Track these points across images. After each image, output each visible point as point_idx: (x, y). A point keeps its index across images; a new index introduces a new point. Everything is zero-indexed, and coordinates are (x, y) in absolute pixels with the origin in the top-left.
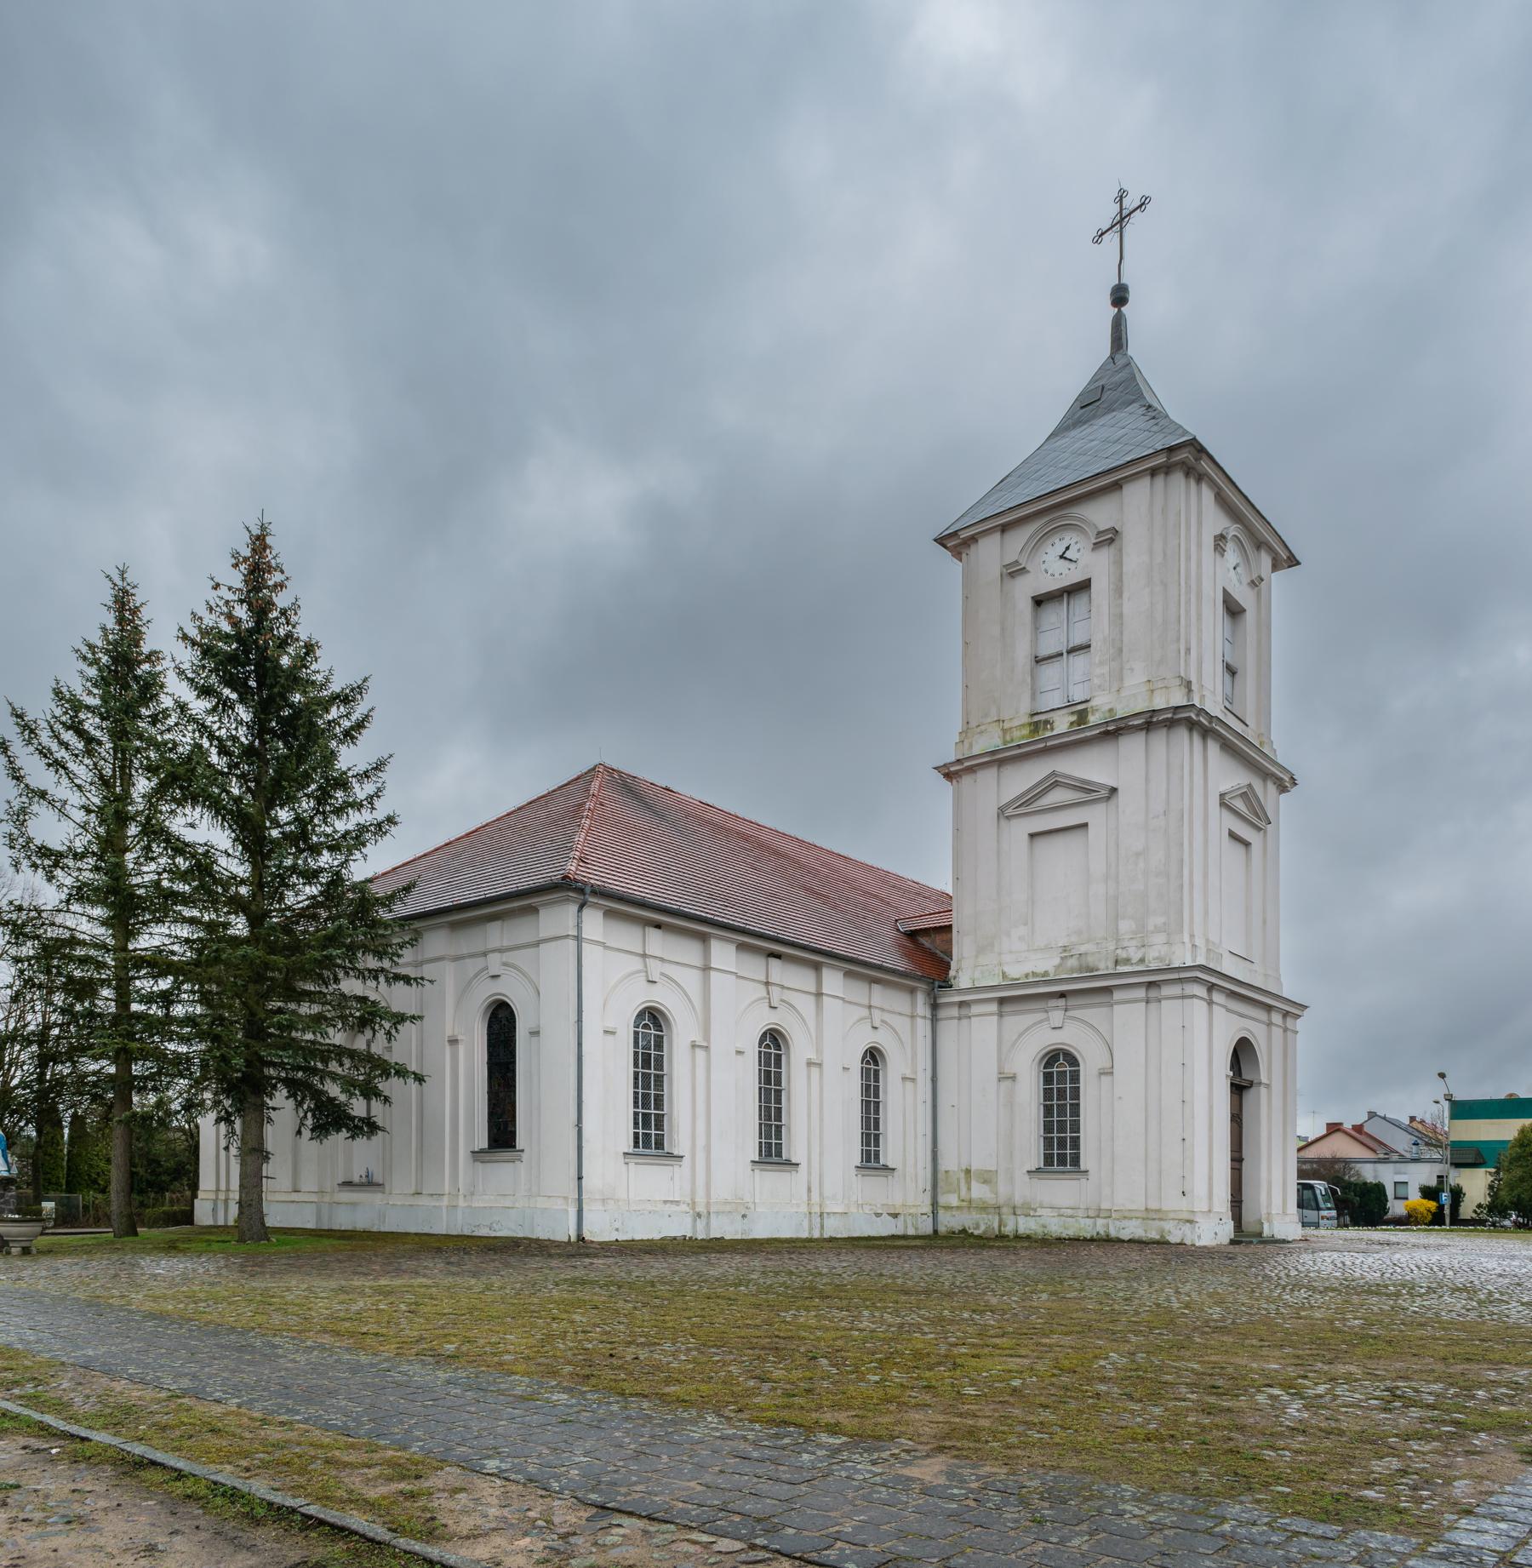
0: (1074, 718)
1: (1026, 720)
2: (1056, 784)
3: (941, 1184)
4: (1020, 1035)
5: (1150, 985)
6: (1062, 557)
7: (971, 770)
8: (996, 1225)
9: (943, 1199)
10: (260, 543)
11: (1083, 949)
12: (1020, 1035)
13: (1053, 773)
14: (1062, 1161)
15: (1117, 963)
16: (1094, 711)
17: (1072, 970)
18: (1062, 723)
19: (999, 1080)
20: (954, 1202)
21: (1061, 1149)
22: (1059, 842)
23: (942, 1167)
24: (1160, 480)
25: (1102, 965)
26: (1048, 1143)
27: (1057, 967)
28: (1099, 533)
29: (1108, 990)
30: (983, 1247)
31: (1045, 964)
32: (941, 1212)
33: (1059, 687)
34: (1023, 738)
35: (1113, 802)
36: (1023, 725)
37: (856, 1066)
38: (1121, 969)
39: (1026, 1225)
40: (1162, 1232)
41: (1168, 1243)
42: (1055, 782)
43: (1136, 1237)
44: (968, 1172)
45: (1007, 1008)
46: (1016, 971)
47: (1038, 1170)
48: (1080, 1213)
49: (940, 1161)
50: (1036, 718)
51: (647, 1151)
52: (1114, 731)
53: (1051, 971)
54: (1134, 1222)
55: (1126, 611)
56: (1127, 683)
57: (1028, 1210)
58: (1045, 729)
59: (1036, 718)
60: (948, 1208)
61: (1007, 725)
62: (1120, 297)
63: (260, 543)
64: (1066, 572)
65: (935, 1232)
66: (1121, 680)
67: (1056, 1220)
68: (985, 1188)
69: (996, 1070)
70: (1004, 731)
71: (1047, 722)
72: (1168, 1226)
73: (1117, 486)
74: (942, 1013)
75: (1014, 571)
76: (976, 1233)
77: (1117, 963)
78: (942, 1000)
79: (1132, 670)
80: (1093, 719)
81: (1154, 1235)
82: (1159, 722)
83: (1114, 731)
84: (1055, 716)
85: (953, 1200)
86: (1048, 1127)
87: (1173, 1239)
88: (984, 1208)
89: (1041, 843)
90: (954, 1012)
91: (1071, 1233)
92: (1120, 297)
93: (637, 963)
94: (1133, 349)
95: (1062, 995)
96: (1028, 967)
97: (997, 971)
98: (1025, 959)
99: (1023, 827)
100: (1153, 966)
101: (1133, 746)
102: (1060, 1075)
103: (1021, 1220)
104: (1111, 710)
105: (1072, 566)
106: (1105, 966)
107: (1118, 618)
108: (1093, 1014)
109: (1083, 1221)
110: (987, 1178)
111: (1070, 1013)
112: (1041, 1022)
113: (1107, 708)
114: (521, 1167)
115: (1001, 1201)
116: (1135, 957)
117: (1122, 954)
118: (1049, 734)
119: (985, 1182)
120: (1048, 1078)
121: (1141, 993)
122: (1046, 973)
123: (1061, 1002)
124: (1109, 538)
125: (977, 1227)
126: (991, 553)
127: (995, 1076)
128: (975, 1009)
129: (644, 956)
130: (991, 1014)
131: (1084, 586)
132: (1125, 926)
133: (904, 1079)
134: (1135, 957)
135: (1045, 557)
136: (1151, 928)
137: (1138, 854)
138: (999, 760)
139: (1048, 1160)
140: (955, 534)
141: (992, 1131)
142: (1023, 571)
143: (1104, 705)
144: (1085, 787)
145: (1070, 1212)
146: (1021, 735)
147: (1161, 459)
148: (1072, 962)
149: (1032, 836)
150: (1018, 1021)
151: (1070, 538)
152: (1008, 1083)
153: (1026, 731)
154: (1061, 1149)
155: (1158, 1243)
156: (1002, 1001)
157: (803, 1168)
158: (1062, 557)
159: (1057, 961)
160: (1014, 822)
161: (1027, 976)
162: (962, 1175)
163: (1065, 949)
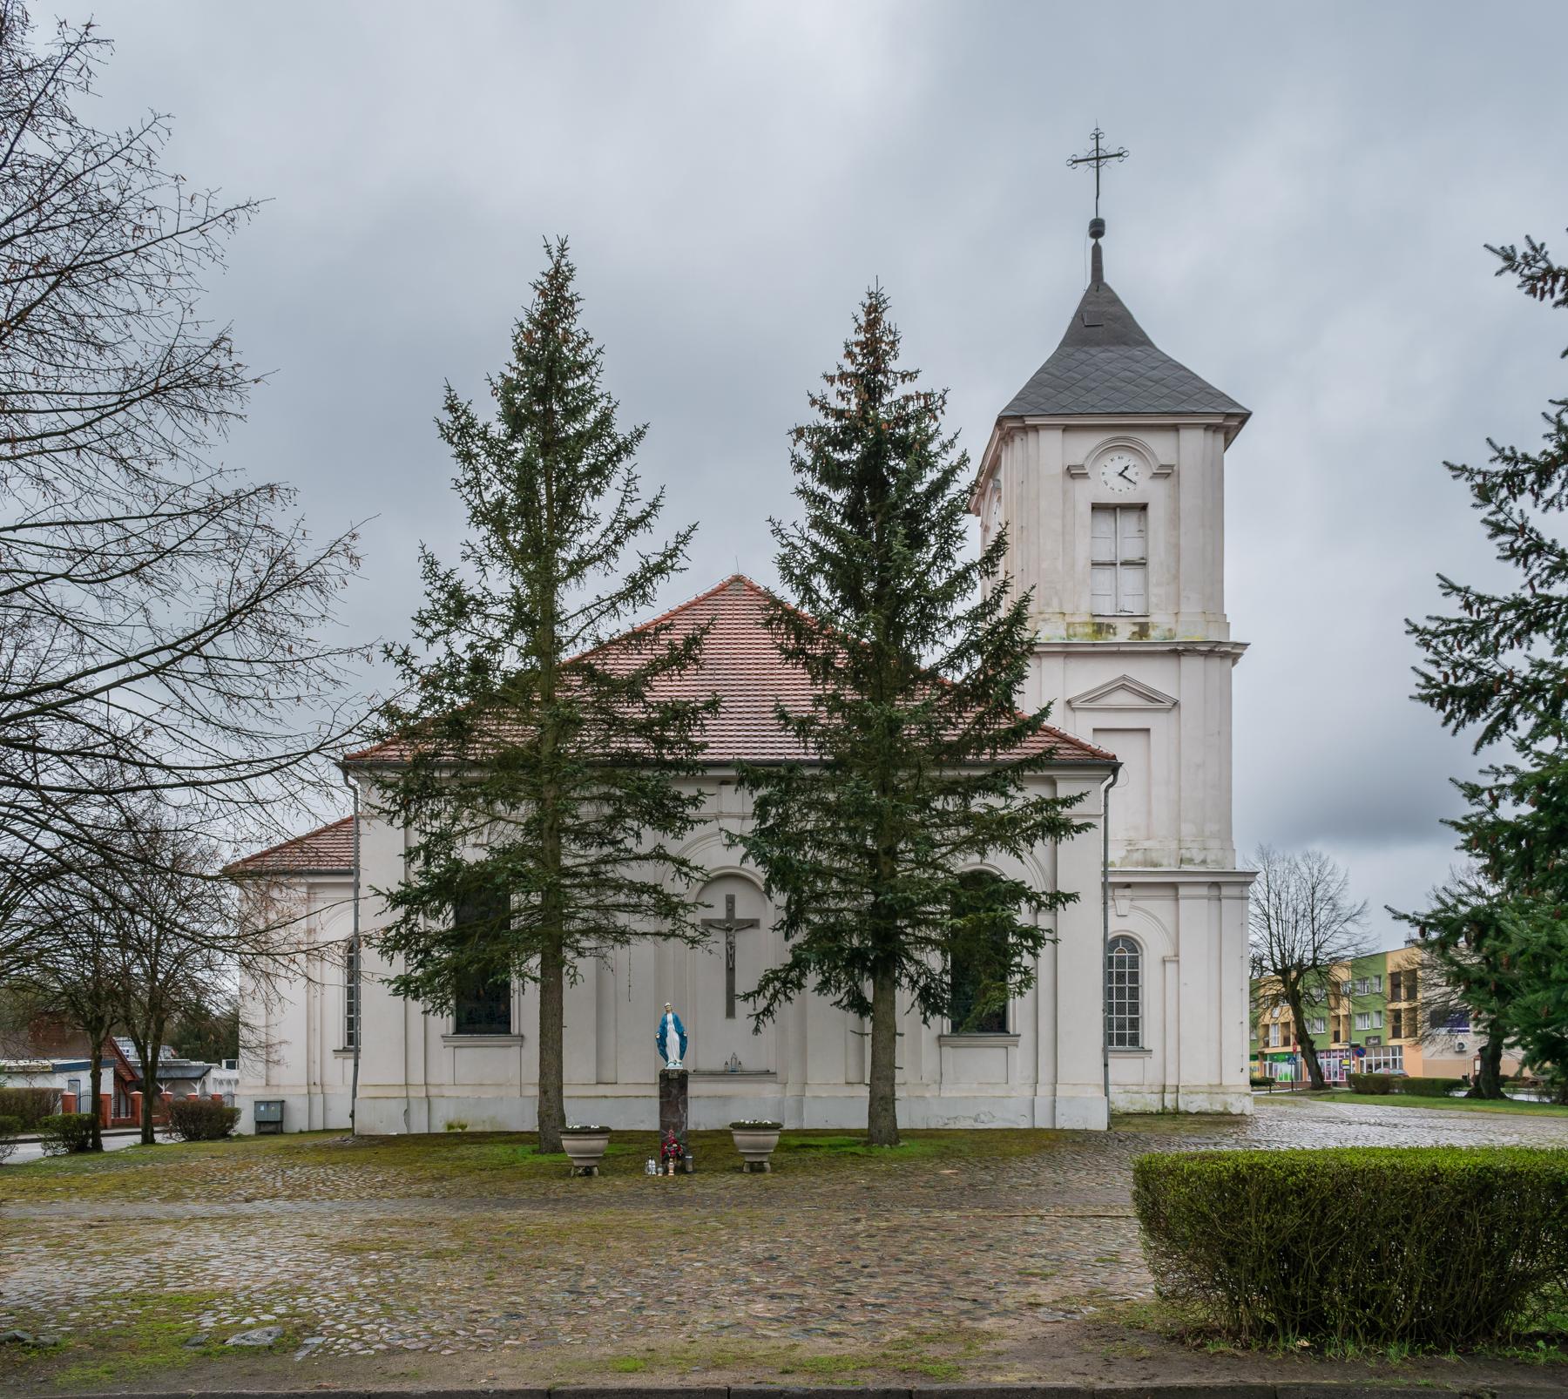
0: (1136, 629)
1: (1088, 619)
2: (1123, 687)
5: (1217, 885)
10: (874, 310)
11: (1147, 844)
13: (1124, 678)
17: (1138, 864)
18: (1124, 633)
24: (1210, 434)
25: (1165, 862)
27: (1124, 859)
28: (1162, 466)
29: (1175, 886)
30: (1217, 1124)
35: (1174, 713)
38: (1186, 868)
40: (1225, 1104)
41: (1230, 1114)
48: (1145, 1089)
50: (1098, 620)
52: (1178, 652)
54: (1201, 1097)
55: (1183, 542)
61: (1069, 619)
62: (1097, 229)
63: (874, 310)
66: (1178, 605)
67: (1123, 1096)
71: (1109, 626)
72: (1230, 1099)
75: (1074, 473)
81: (1219, 1108)
83: (1178, 652)
84: (1117, 622)
87: (1235, 1111)
91: (1137, 1108)
92: (1097, 229)
94: (1109, 278)
95: (1128, 886)
105: (1131, 486)
108: (1160, 906)
111: (1137, 903)
114: (1020, 1055)
116: (1198, 859)
117: (1187, 855)
121: (1204, 891)
123: (1127, 892)
124: (1165, 473)
131: (1143, 508)
135: (1104, 470)
143: (1162, 625)
144: (1151, 697)
145: (1135, 1088)
146: (1083, 635)
147: (1219, 420)
148: (1138, 856)
151: (1127, 459)
153: (1089, 630)
155: (1222, 1114)
157: (1157, 1055)
159: (1124, 853)
160: (1078, 714)
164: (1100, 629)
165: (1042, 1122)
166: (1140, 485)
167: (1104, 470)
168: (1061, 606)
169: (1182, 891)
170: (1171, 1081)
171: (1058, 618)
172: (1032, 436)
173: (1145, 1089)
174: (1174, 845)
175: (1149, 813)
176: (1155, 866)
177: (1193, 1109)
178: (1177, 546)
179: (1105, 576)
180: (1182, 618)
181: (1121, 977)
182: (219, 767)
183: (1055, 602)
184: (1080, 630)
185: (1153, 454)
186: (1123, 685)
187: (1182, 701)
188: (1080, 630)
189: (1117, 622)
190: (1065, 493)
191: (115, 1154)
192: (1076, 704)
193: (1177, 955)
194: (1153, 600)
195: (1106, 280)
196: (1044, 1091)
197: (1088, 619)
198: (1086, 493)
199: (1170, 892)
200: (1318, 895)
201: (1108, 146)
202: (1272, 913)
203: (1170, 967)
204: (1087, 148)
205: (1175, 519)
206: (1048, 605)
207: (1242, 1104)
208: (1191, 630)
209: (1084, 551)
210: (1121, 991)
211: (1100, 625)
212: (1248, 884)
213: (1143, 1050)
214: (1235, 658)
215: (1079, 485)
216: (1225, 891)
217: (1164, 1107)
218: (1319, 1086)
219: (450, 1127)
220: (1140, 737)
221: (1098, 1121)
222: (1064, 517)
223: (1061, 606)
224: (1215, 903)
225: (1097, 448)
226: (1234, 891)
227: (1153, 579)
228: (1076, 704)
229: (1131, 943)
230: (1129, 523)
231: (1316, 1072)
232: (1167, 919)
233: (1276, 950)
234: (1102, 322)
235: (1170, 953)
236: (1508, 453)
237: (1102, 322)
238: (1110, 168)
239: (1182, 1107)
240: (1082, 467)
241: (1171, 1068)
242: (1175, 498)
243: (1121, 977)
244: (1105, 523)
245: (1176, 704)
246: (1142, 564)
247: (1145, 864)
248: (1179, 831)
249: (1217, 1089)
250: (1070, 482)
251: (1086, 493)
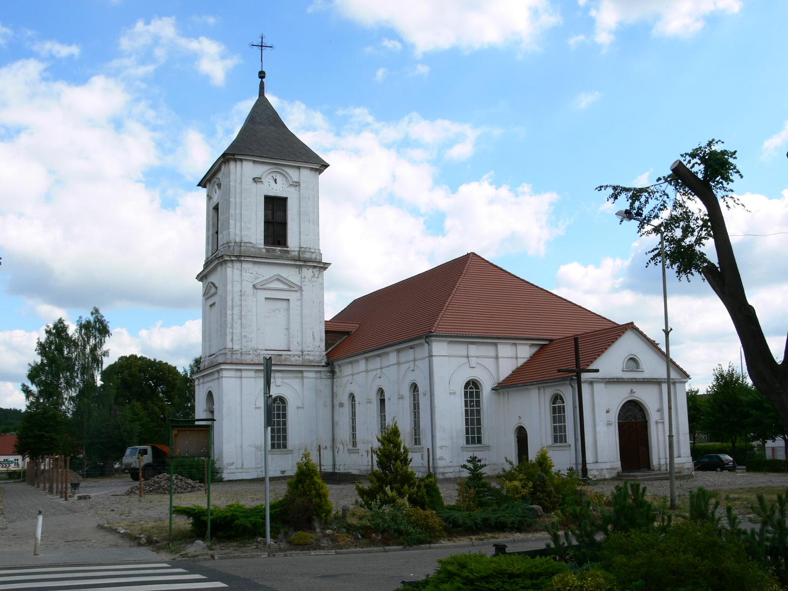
2: (278, 279)
14: (279, 447)
37: (460, 390)
42: (279, 279)
62: (262, 75)
75: (256, 180)
92: (262, 75)
93: (466, 360)
111: (286, 381)
124: (297, 184)
129: (468, 357)
133: (298, 408)
160: (258, 291)
169: (305, 374)
172: (239, 164)
182: (233, 318)
186: (279, 279)
191: (37, 518)
192: (258, 286)
199: (300, 375)
204: (267, 42)
210: (279, 437)
214: (325, 268)
215: (259, 185)
216: (244, 374)
219: (283, 472)
225: (268, 169)
229: (282, 400)
236: (701, 245)
238: (266, 51)
240: (260, 178)
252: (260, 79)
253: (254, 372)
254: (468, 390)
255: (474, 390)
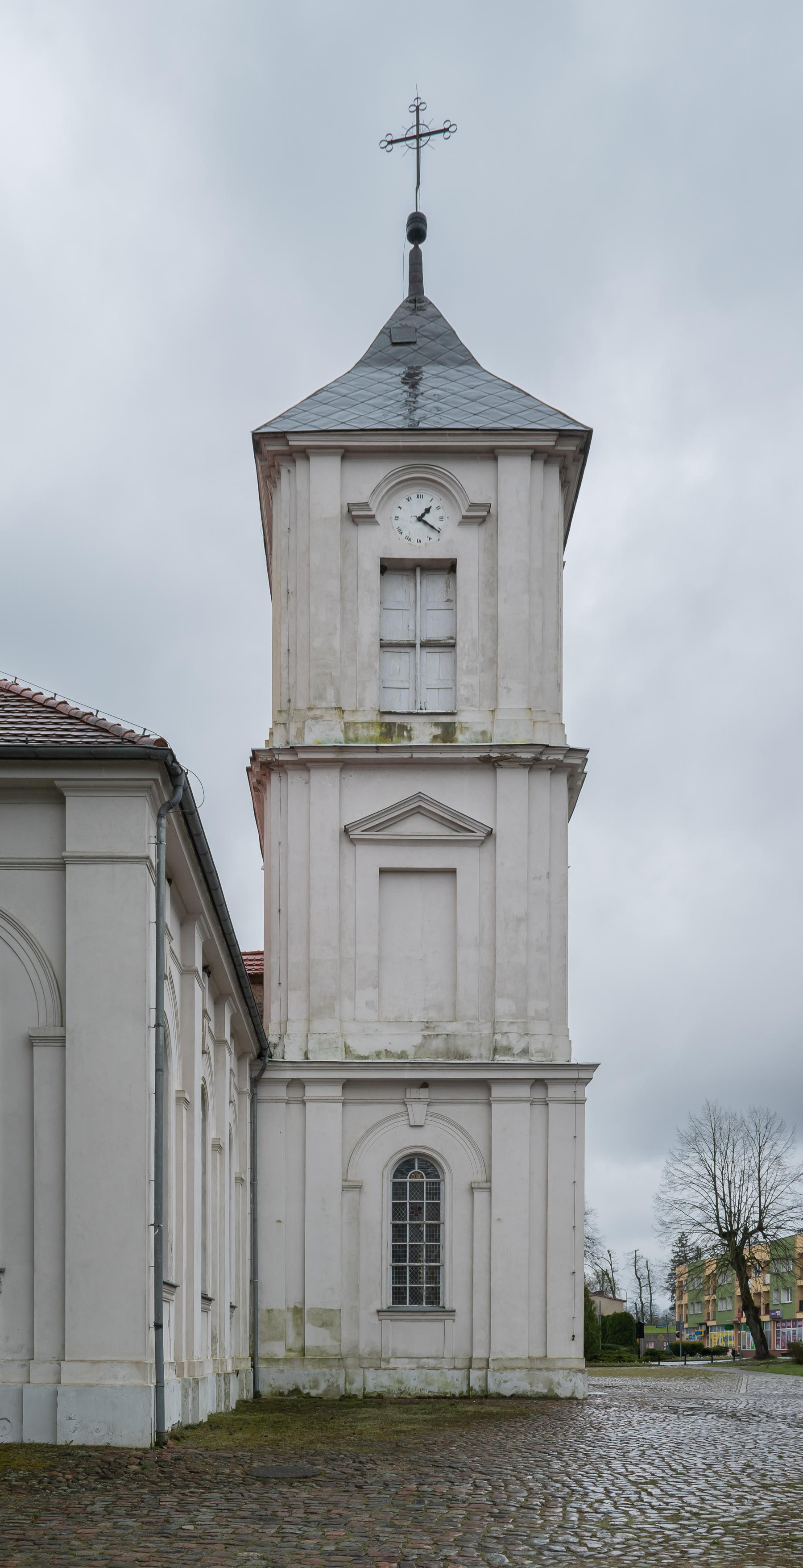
0: (438, 731)
1: (373, 717)
2: (418, 811)
3: (261, 1327)
4: (369, 1132)
6: (420, 519)
7: (305, 766)
8: (341, 1382)
9: (263, 1350)
11: (451, 1028)
12: (369, 1132)
13: (419, 796)
14: (416, 1297)
15: (495, 1050)
16: (464, 728)
17: (437, 1054)
18: (423, 734)
19: (344, 1188)
20: (281, 1353)
21: (416, 1281)
22: (413, 885)
23: (263, 1306)
24: (539, 466)
25: (474, 1052)
26: (398, 1274)
27: (419, 1048)
28: (473, 506)
29: (485, 1084)
31: (406, 1042)
32: (262, 1366)
33: (418, 687)
34: (372, 739)
35: (489, 846)
36: (371, 724)
38: (500, 1059)
39: (375, 1381)
40: (550, 1383)
41: (556, 1398)
42: (418, 807)
43: (520, 1391)
44: (298, 1312)
45: (352, 1095)
46: (363, 1047)
47: (389, 1310)
48: (445, 1364)
49: (260, 1297)
50: (388, 719)
51: (416, 1306)
52: (493, 760)
53: (411, 1052)
54: (518, 1374)
55: (502, 612)
56: (502, 704)
57: (378, 1361)
58: (401, 736)
59: (388, 719)
60: (272, 1361)
61: (348, 718)
62: (417, 230)
64: (425, 540)
65: (257, 1394)
66: (496, 699)
68: (325, 1332)
69: (339, 1177)
70: (347, 726)
71: (402, 727)
72: (558, 1377)
73: (491, 455)
74: (264, 1092)
75: (357, 516)
76: (314, 1393)
77: (495, 1050)
78: (268, 1075)
79: (509, 690)
80: (462, 739)
81: (541, 1389)
82: (548, 762)
83: (493, 760)
84: (415, 723)
85: (278, 1350)
86: (398, 1254)
87: (563, 1393)
88: (323, 1360)
89: (394, 884)
90: (282, 1092)
91: (434, 1389)
92: (417, 230)
94: (429, 292)
95: (424, 1084)
96: (380, 1044)
97: (341, 1044)
98: (377, 1032)
99: (373, 858)
100: (536, 1059)
101: (512, 783)
102: (417, 1187)
103: (370, 1374)
104: (484, 733)
105: (433, 535)
106: (479, 1054)
107: (492, 620)
108: (466, 1113)
109: (450, 1374)
110: (327, 1320)
111: (435, 1109)
112: (397, 1115)
113: (480, 728)
115: (344, 1351)
116: (518, 1047)
117: (502, 1041)
118: (405, 743)
119: (324, 1325)
120: (398, 1190)
121: (524, 1092)
122: (403, 1054)
123: (424, 1093)
124: (480, 516)
125: (316, 1386)
126: (325, 485)
127: (339, 1184)
128: (312, 1092)
130: (334, 1100)
131: (449, 567)
132: (504, 1007)
134: (518, 1047)
135: (398, 513)
136: (531, 1013)
137: (519, 920)
138: (345, 760)
139: (398, 1296)
140: (282, 436)
141: (338, 1256)
142: (371, 519)
143: (474, 725)
145: (432, 1362)
146: (369, 736)
147: (548, 442)
148: (437, 1044)
149: (383, 871)
150: (368, 1113)
152: (354, 1194)
153: (375, 732)
154: (416, 1281)
155: (544, 1398)
156: (347, 1084)
158: (420, 519)
159: (418, 1040)
160: (361, 849)
161: (378, 1054)
162: (289, 1316)
163: (428, 1025)
164: (388, 730)
165: (35, 1434)
166: (446, 535)
167: (398, 513)
168: (338, 701)
169: (497, 1092)
170: (479, 1353)
171: (334, 716)
172: (300, 465)
173: (445, 1364)
174: (486, 1030)
175: (455, 986)
176: (461, 1057)
177: (507, 1390)
178: (494, 619)
179: (399, 662)
180: (500, 716)
181: (416, 1210)
183: (330, 694)
184: (363, 732)
185: (461, 489)
187: (499, 831)
188: (363, 732)
189: (415, 723)
190: (345, 544)
192: (356, 834)
193: (489, 1180)
194: (462, 692)
195: (426, 294)
196: (41, 1373)
197: (373, 717)
198: (373, 544)
199: (480, 1095)
200: (765, 1153)
201: (431, 120)
202: (718, 1173)
203: (480, 1197)
205: (491, 583)
206: (321, 697)
207: (573, 1379)
208: (512, 729)
209: (368, 628)
211: (389, 725)
212: (587, 1081)
213: (444, 1311)
216: (555, 1092)
217: (470, 1388)
218: (763, 1355)
220: (445, 880)
221: (136, 1433)
222: (342, 577)
223: (338, 701)
224: (539, 1109)
225: (386, 479)
226: (565, 1092)
227: (462, 664)
228: (356, 834)
230: (433, 589)
231: (761, 1341)
232: (477, 1132)
233: (722, 1214)
234: (416, 339)
235: (480, 1177)
237: (416, 339)
238: (434, 147)
239: (492, 1388)
241: (480, 1335)
242: (492, 552)
243: (416, 1210)
244: (401, 590)
245: (490, 834)
246: (450, 645)
247: (447, 1054)
248: (493, 1011)
249: (538, 1364)
250: (351, 530)
251: (373, 544)
252: (412, 246)
253: (338, 459)
254: (408, 1179)
255: (425, 1179)
